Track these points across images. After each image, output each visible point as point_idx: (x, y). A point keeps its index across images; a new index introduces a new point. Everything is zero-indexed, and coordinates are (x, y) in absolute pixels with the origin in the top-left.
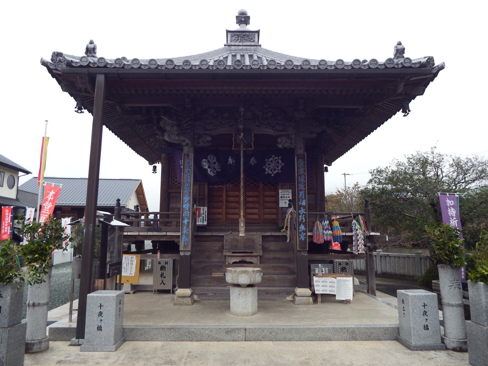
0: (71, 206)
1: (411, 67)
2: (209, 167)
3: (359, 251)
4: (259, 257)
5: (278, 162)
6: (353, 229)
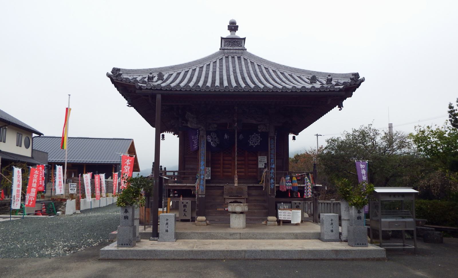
0: (73, 163)
1: (334, 91)
2: (212, 141)
3: (308, 196)
4: (245, 199)
5: (258, 138)
6: (305, 183)
